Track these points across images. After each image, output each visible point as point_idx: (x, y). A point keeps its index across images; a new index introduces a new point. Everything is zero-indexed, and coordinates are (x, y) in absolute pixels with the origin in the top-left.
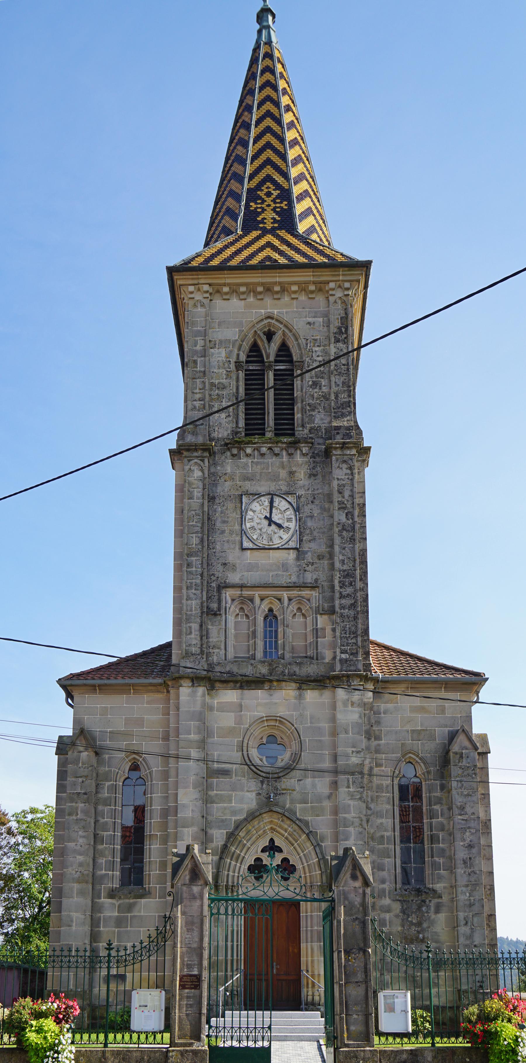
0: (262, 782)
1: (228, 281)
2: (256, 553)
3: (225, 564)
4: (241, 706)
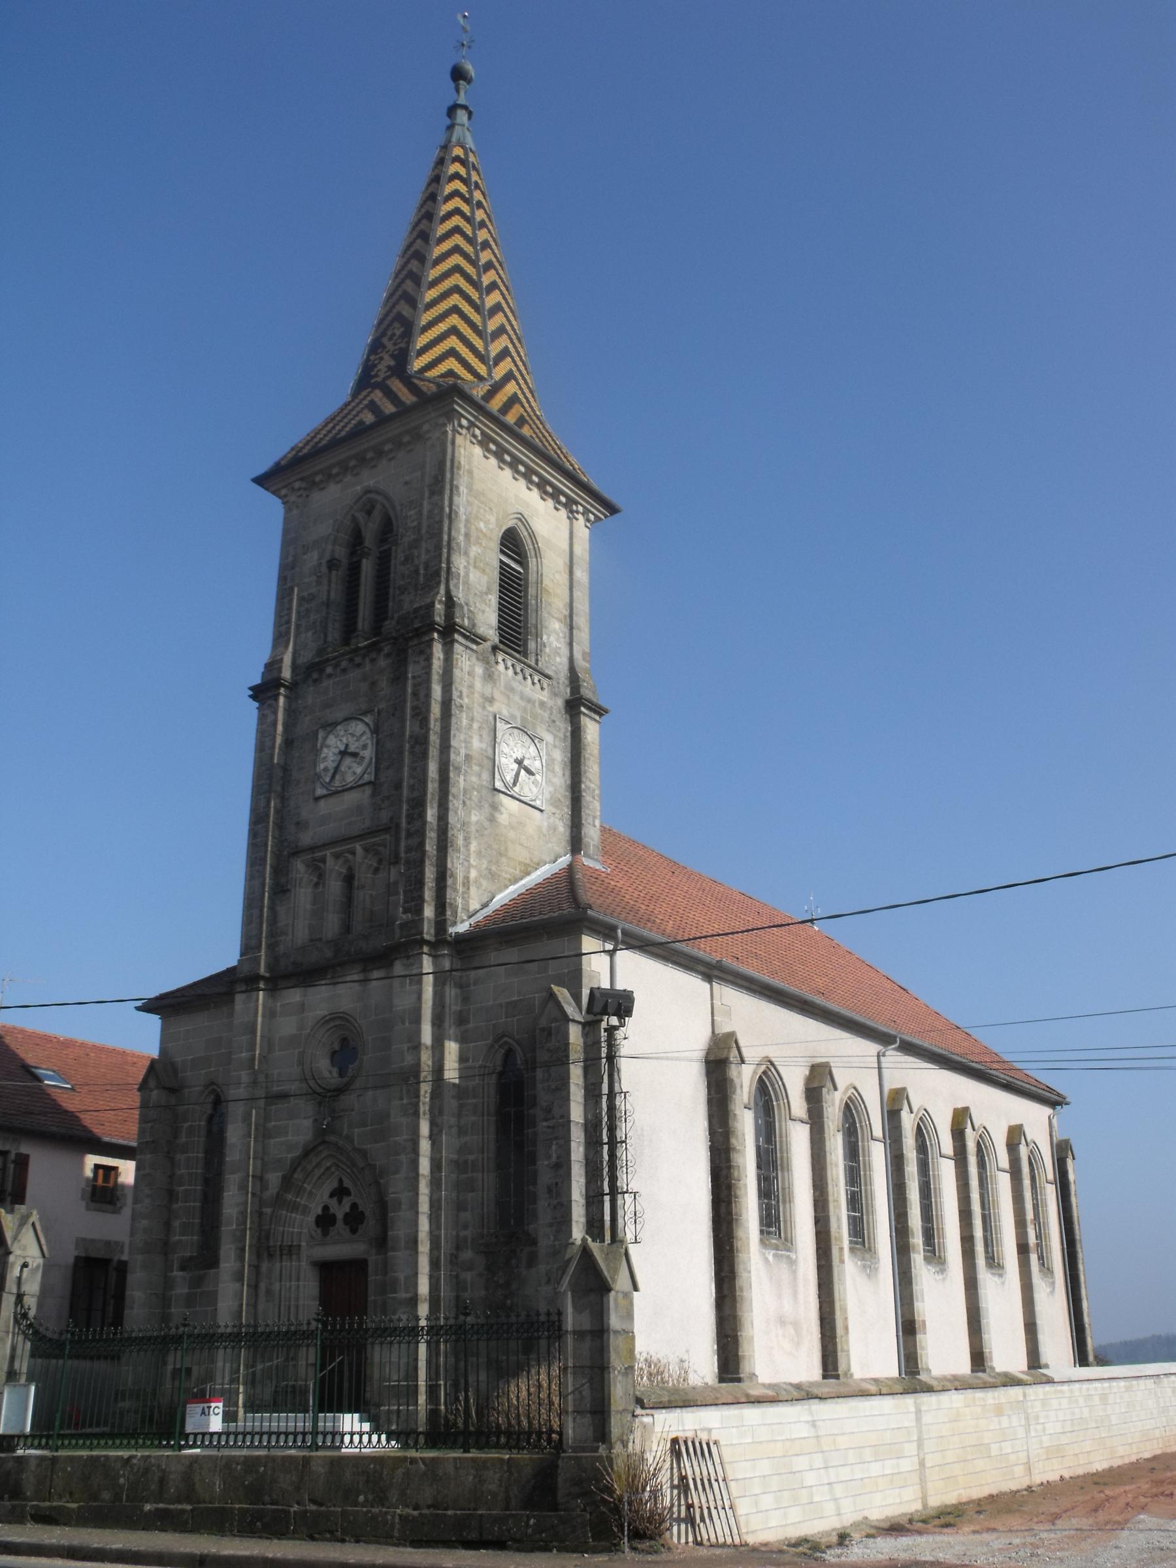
0: (320, 1104)
2: (332, 800)
3: (298, 824)
4: (303, 1005)
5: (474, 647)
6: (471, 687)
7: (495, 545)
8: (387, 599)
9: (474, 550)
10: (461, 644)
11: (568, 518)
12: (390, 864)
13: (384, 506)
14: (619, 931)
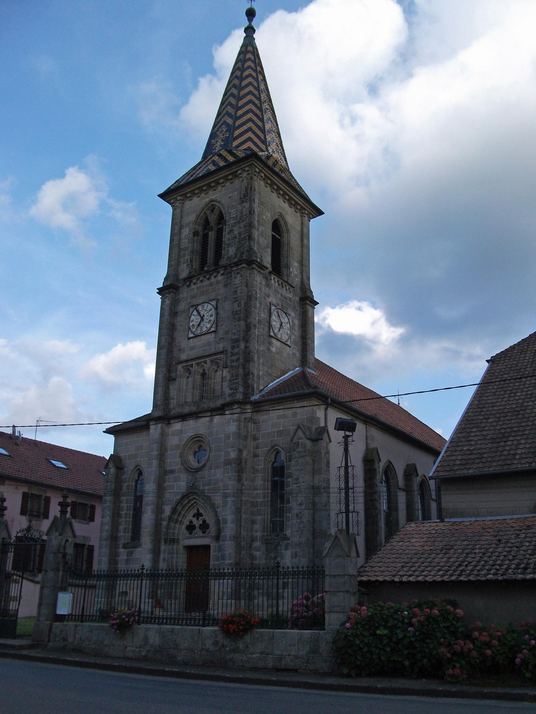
1: (188, 190)
2: (195, 339)
3: (180, 350)
5: (262, 271)
6: (260, 289)
7: (270, 226)
8: (221, 250)
9: (261, 228)
10: (257, 270)
11: (301, 216)
12: (223, 368)
13: (219, 208)
14: (329, 400)
